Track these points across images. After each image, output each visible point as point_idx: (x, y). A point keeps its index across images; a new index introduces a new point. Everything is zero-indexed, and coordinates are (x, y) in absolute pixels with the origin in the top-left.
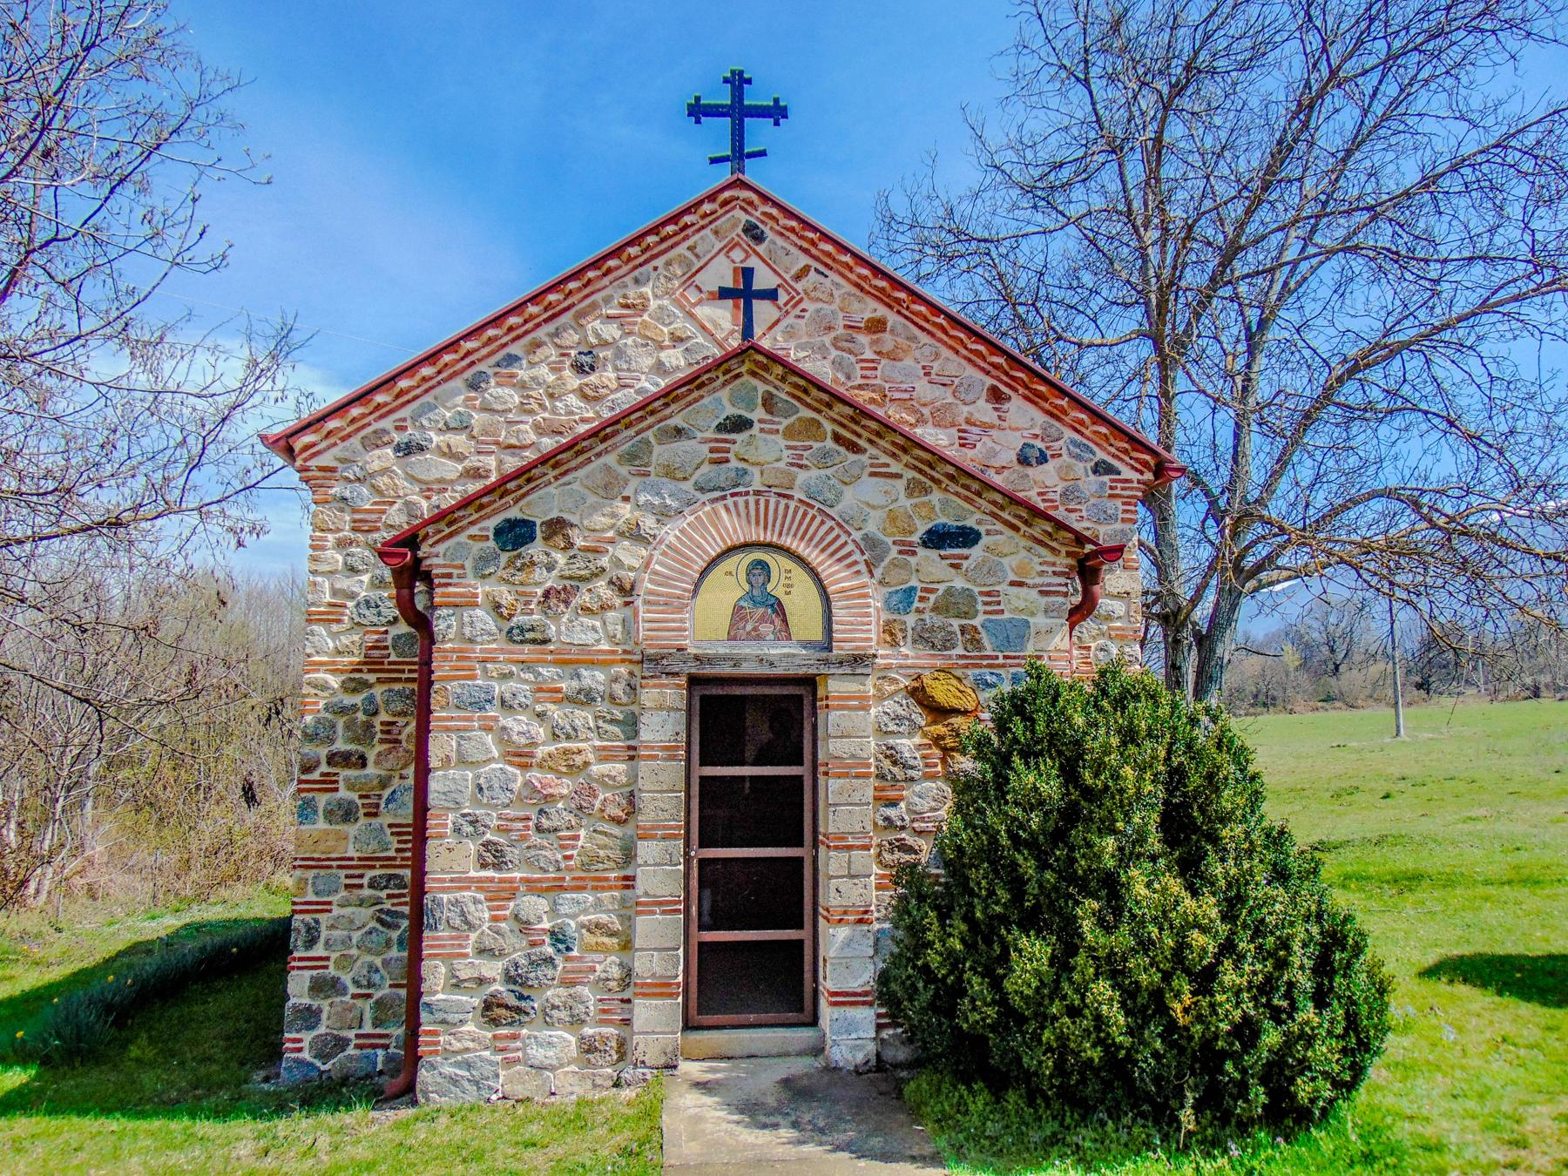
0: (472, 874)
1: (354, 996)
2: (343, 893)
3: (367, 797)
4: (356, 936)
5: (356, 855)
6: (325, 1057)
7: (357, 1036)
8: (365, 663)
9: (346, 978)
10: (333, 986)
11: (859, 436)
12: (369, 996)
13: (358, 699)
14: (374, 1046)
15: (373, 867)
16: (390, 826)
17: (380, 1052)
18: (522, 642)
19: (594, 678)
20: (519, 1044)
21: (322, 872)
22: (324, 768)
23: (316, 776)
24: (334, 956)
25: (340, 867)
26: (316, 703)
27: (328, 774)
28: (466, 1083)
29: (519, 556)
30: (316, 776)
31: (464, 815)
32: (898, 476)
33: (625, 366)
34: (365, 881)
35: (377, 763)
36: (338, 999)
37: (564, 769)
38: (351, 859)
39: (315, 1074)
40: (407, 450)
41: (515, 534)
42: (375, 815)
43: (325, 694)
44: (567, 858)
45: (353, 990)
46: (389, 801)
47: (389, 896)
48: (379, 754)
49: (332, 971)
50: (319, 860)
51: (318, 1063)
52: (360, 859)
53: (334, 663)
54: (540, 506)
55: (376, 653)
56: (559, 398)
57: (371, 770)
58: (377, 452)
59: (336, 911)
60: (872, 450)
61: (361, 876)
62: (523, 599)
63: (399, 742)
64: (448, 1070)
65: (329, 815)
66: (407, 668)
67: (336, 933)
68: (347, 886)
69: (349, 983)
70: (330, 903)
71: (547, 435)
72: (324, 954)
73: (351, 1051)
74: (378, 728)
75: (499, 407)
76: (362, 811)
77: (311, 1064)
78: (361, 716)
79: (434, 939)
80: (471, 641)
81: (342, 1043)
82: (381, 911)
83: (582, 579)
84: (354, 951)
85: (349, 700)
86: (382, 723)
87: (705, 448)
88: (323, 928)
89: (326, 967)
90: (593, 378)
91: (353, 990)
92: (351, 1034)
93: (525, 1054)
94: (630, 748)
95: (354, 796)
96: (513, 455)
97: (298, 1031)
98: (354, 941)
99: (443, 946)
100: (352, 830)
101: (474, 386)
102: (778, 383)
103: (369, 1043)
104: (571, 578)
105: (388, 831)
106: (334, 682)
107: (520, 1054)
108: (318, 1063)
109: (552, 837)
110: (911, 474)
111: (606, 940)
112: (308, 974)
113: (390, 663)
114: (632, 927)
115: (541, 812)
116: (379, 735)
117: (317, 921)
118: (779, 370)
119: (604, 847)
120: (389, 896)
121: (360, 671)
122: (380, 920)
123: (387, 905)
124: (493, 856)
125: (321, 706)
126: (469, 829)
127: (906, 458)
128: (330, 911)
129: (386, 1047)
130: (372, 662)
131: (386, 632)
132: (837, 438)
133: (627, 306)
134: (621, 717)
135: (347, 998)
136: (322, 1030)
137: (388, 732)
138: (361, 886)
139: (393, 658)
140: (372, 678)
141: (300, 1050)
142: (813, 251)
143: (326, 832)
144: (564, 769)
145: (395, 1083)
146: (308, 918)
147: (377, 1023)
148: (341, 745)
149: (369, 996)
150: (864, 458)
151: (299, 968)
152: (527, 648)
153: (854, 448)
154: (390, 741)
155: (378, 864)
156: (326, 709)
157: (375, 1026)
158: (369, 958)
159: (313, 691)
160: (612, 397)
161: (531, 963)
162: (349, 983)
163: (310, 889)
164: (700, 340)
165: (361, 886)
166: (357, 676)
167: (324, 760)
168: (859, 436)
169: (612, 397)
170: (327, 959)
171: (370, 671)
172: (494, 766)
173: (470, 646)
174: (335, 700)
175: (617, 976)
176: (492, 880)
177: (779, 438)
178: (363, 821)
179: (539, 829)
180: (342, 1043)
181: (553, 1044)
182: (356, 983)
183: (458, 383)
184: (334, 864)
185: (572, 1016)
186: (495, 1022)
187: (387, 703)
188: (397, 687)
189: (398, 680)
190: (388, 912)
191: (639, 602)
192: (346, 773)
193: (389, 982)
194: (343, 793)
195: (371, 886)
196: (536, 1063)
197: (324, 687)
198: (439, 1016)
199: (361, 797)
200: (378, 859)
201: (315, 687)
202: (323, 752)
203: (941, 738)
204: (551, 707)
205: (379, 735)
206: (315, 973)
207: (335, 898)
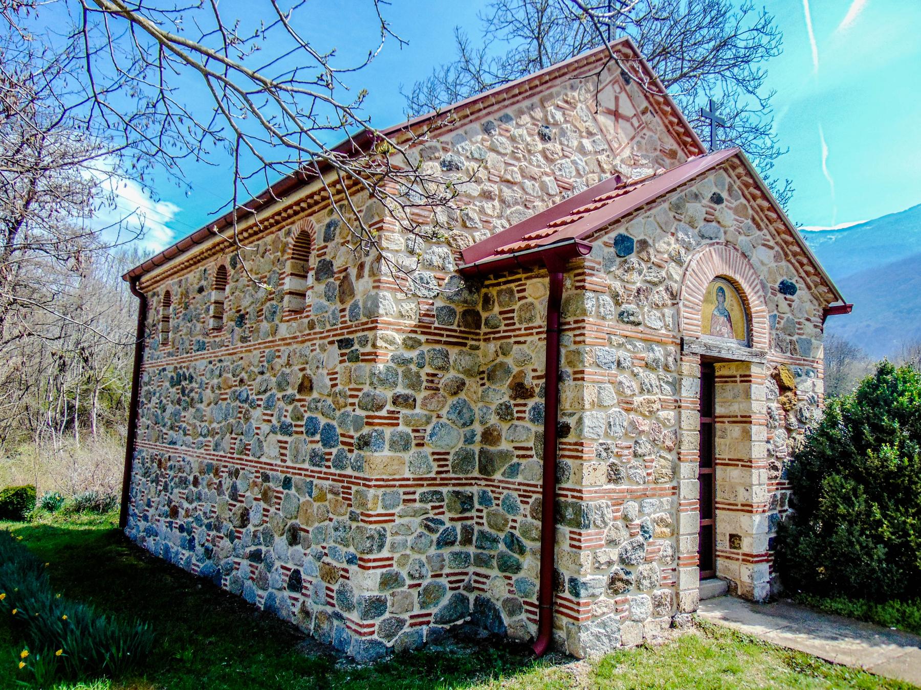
0: (605, 487)
1: (411, 586)
2: (401, 507)
3: (418, 431)
4: (410, 539)
5: (411, 476)
6: (389, 636)
7: (412, 617)
8: (419, 327)
9: (404, 573)
10: (396, 580)
11: (762, 220)
12: (419, 585)
13: (414, 354)
14: (421, 624)
15: (422, 485)
16: (433, 454)
17: (425, 627)
18: (628, 323)
19: (659, 352)
20: (627, 606)
21: (388, 490)
22: (389, 407)
23: (384, 413)
24: (396, 556)
25: (401, 486)
26: (385, 355)
27: (393, 412)
28: (603, 637)
29: (625, 262)
30: (384, 413)
31: (601, 444)
32: (772, 248)
33: (566, 143)
34: (417, 496)
35: (424, 405)
36: (399, 590)
37: (647, 413)
38: (408, 480)
39: (383, 651)
40: (449, 166)
41: (624, 246)
42: (422, 445)
43: (392, 348)
44: (648, 474)
45: (409, 582)
46: (431, 436)
47: (433, 508)
48: (425, 398)
49: (395, 568)
50: (388, 480)
51: (385, 641)
52: (414, 479)
53: (399, 324)
54: (636, 230)
55: (427, 319)
56: (533, 154)
57: (418, 410)
58: (430, 163)
59: (398, 521)
60: (765, 231)
61: (414, 493)
62: (627, 292)
63: (438, 389)
64: (595, 630)
65: (393, 445)
66: (445, 333)
67: (399, 538)
68: (405, 501)
69: (405, 576)
70: (393, 515)
71: (527, 178)
72: (389, 555)
73: (406, 629)
74: (424, 378)
75: (503, 151)
76: (414, 442)
77: (380, 643)
78: (413, 368)
79: (588, 535)
80: (604, 318)
81: (401, 623)
82: (427, 519)
83: (655, 284)
84: (408, 552)
85: (408, 354)
86: (428, 375)
87: (704, 210)
88: (388, 534)
89: (391, 565)
90: (549, 145)
91: (409, 582)
92: (406, 616)
93: (630, 612)
94: (676, 401)
95: (408, 430)
96: (509, 188)
97: (373, 618)
98: (409, 544)
99: (591, 540)
100: (407, 456)
101: (487, 130)
102: (736, 178)
103: (419, 620)
104: (649, 282)
105: (431, 458)
106: (399, 338)
107: (627, 613)
108: (385, 641)
109: (641, 459)
110: (777, 248)
111: (664, 529)
112: (379, 571)
113: (436, 328)
114: (678, 521)
115: (636, 442)
116: (425, 384)
117: (385, 530)
118: (741, 170)
119: (663, 467)
120: (433, 508)
121: (416, 332)
122: (427, 527)
123: (431, 515)
124: (614, 476)
125: (389, 358)
126: (604, 454)
127: (778, 239)
128: (393, 521)
129: (428, 623)
130: (423, 327)
131: (433, 304)
132: (753, 219)
133: (566, 102)
134: (671, 380)
135: (405, 588)
136: (387, 615)
137: (432, 382)
138: (414, 500)
139: (436, 325)
140: (423, 338)
141: (373, 633)
142: (651, 99)
143: (392, 459)
144: (647, 413)
145: (548, 646)
146: (378, 527)
147: (423, 605)
148: (401, 390)
149: (419, 585)
150: (761, 233)
151: (374, 568)
152: (629, 327)
153: (759, 227)
154: (433, 389)
155: (425, 483)
156: (393, 360)
157: (422, 608)
158: (417, 556)
159: (384, 345)
160: (559, 161)
161: (633, 548)
162: (405, 576)
163: (380, 504)
164: (599, 137)
165: (414, 500)
166: (413, 335)
167: (390, 401)
168: (762, 220)
169: (559, 161)
170: (391, 559)
171: (423, 333)
172: (614, 409)
173: (602, 322)
174: (398, 353)
175: (671, 554)
176: (614, 491)
177: (731, 212)
178: (414, 450)
179: (635, 455)
180: (401, 623)
181: (640, 603)
182: (412, 576)
183: (477, 126)
184: (397, 483)
185: (651, 583)
186: (616, 592)
187: (432, 359)
188: (438, 347)
189: (439, 342)
190: (432, 520)
191: (681, 305)
192: (404, 411)
193: (430, 574)
194: (402, 428)
195: (421, 501)
196: (636, 617)
197: (392, 342)
198: (591, 591)
199: (414, 431)
200: (426, 479)
201: (386, 341)
202: (389, 394)
203: (784, 404)
204: (641, 370)
205: (425, 384)
206: (384, 570)
207: (396, 511)
